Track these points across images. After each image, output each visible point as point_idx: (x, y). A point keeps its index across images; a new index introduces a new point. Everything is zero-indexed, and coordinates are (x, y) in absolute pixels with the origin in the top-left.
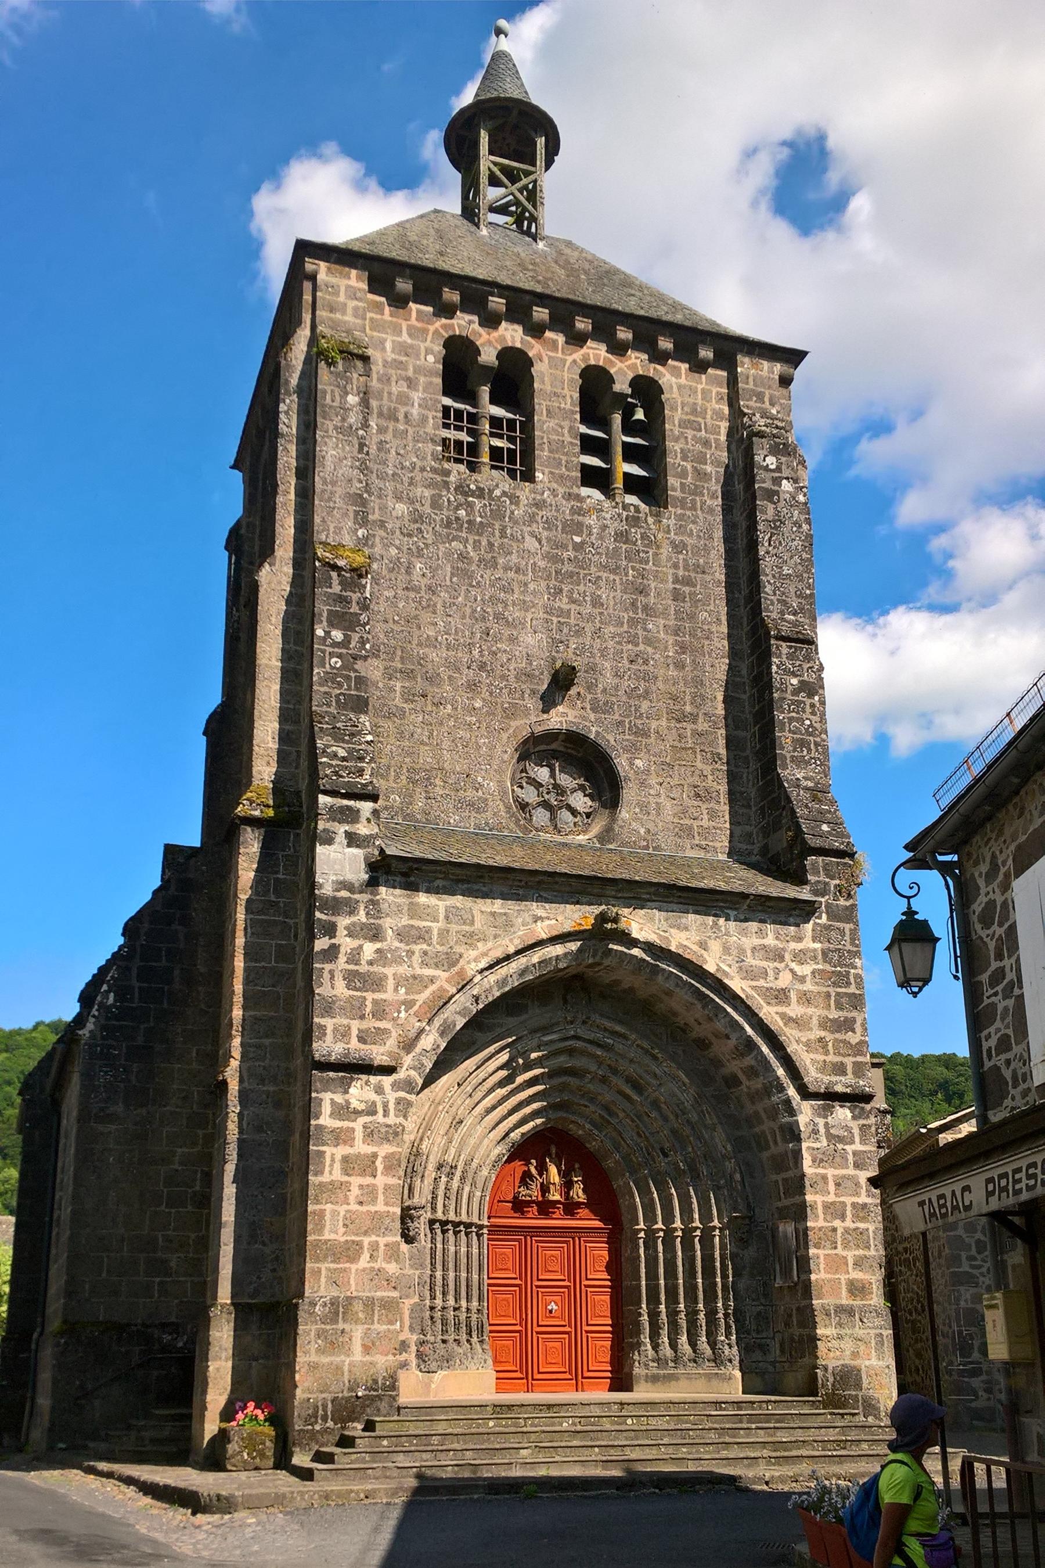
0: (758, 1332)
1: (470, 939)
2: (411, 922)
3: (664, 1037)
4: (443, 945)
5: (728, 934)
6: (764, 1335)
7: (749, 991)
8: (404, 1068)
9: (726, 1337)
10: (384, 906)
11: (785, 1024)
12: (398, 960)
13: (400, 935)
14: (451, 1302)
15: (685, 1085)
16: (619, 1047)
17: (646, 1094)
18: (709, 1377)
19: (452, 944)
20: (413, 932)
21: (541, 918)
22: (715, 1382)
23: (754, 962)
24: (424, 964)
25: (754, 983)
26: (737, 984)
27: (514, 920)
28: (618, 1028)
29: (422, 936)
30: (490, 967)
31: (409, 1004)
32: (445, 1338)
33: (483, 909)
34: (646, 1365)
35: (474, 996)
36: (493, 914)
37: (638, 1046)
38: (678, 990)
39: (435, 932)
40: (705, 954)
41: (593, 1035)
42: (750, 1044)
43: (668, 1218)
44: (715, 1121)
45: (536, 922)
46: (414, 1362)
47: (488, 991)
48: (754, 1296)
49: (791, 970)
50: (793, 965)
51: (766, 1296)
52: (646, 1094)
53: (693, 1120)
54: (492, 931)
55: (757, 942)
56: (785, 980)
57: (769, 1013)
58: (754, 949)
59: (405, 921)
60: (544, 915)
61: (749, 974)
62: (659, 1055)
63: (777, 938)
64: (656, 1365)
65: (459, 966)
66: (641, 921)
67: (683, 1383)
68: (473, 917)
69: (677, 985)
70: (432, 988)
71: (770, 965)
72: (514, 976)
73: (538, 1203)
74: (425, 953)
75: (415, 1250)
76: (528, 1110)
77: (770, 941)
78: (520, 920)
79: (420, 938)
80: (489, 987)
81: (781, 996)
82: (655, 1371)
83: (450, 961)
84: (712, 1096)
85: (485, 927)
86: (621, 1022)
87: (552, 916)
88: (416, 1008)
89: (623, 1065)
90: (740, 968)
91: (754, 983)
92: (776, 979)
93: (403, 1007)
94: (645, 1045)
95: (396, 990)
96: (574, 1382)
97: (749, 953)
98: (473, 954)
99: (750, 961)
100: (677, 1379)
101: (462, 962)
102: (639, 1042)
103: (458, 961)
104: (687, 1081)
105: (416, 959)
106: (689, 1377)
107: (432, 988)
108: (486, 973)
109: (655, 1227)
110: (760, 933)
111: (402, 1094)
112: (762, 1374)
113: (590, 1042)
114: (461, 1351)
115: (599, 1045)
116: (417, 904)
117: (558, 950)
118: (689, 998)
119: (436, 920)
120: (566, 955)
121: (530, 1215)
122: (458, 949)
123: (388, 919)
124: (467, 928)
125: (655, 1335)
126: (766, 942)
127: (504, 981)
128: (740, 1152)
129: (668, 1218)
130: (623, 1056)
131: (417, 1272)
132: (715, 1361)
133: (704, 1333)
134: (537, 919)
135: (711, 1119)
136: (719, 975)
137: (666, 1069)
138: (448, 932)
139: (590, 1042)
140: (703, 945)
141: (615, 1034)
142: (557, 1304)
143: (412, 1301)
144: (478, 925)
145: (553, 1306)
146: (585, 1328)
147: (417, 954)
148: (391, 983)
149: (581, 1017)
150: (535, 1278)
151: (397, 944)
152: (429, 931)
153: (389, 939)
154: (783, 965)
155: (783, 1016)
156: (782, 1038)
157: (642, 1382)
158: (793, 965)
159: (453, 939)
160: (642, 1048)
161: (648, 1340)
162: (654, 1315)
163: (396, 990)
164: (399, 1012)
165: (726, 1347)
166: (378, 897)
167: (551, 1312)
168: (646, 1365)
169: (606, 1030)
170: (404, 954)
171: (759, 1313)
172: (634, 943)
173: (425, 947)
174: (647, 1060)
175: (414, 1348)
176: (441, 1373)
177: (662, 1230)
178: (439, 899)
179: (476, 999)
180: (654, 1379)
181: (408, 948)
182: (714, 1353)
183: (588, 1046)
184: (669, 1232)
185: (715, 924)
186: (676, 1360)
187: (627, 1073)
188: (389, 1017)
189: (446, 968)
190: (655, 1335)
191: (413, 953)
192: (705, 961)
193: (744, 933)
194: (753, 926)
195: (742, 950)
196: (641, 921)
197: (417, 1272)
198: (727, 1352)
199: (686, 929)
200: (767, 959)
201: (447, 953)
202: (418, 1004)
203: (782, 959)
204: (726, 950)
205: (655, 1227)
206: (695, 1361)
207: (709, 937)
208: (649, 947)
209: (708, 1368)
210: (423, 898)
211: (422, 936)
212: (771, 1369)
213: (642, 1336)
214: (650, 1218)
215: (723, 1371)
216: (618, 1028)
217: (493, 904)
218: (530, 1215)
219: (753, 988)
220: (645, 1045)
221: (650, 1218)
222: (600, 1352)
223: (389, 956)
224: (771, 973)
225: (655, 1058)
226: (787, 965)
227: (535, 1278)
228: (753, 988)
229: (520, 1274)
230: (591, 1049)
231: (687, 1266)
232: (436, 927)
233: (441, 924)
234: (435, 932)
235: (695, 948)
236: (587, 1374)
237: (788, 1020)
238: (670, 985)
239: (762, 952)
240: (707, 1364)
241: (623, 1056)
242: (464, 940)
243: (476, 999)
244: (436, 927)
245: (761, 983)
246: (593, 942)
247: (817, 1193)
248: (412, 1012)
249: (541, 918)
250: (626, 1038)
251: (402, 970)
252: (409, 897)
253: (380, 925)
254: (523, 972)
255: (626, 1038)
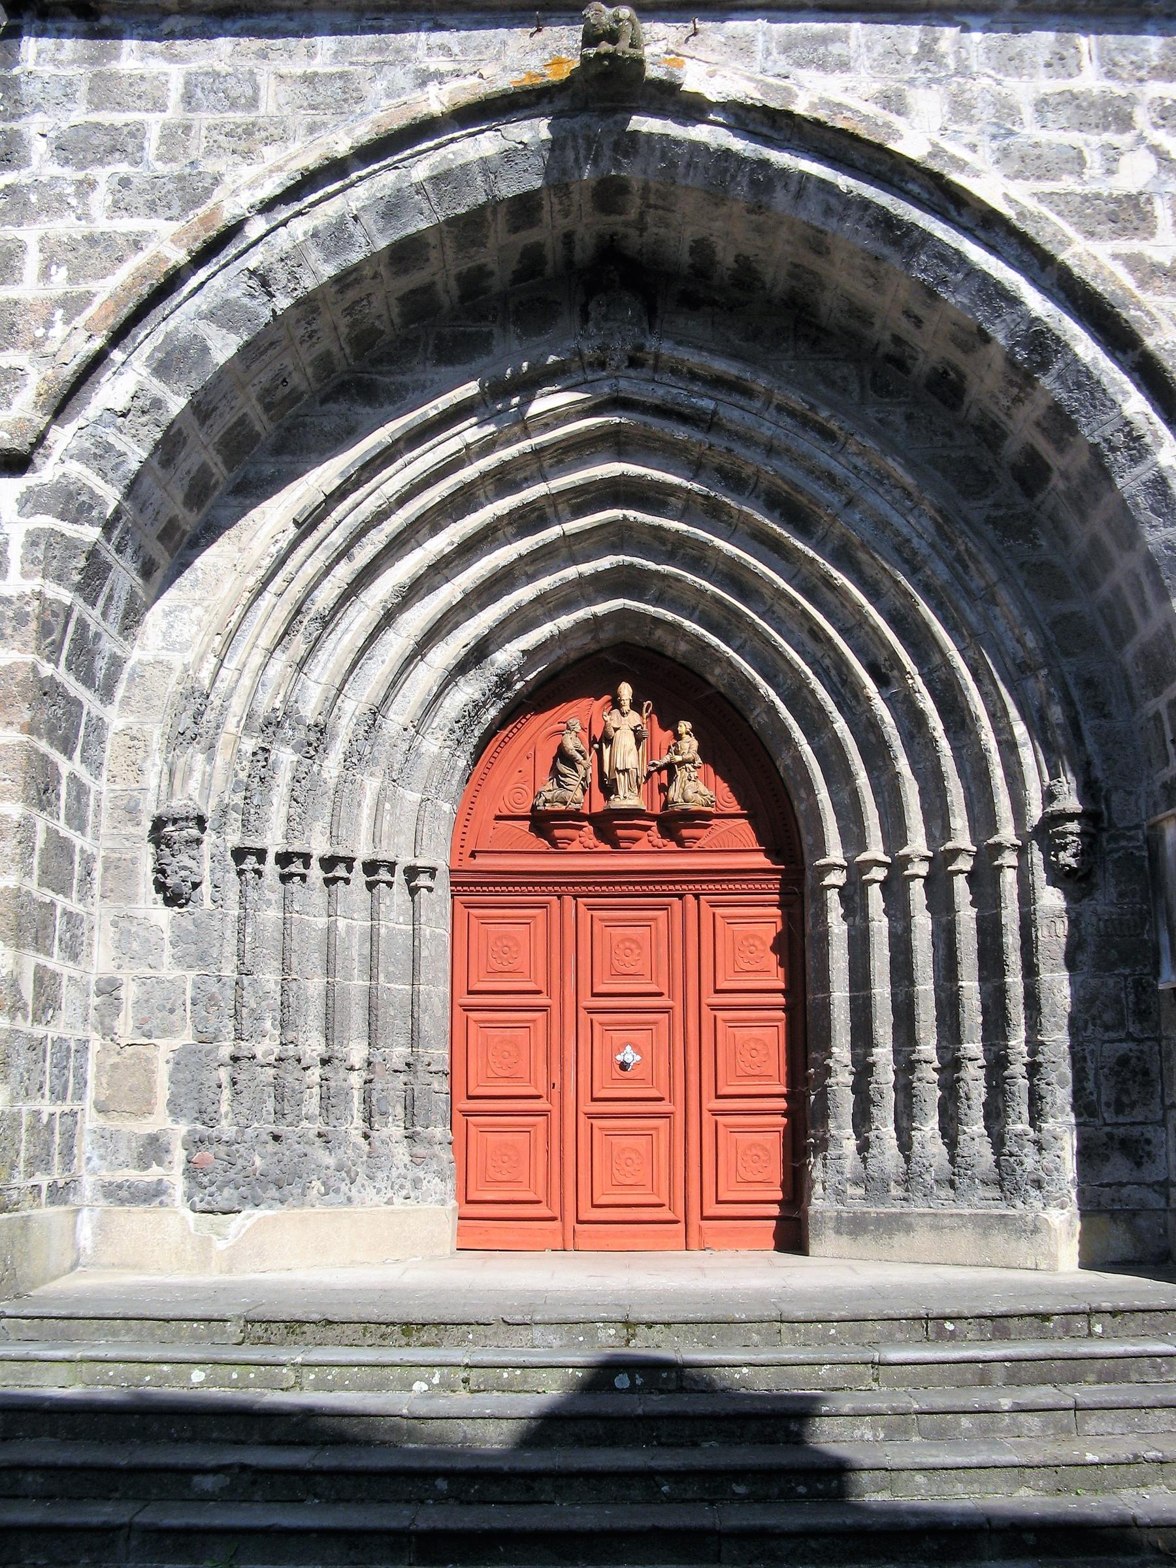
0: (1119, 1107)
1: (246, 140)
2: (95, 117)
3: (854, 386)
4: (173, 159)
5: (963, 70)
6: (1138, 1115)
7: (1032, 205)
8: (55, 458)
9: (1032, 1123)
10: (30, 90)
11: (1142, 284)
12: (55, 205)
13: (64, 149)
14: (313, 1046)
15: (909, 495)
16: (732, 414)
17: (820, 532)
18: (986, 1225)
19: (194, 155)
20: (98, 139)
21: (439, 76)
22: (998, 1239)
23: (1042, 136)
24: (118, 207)
25: (1047, 186)
26: (990, 187)
27: (365, 87)
28: (722, 366)
29: (119, 143)
30: (291, 194)
31: (73, 305)
32: (281, 1129)
33: (284, 71)
34: (840, 1194)
35: (253, 273)
36: (309, 79)
37: (780, 408)
38: (832, 224)
39: (153, 136)
40: (898, 122)
41: (661, 391)
42: (1042, 344)
43: (895, 833)
44: (992, 574)
45: (423, 84)
46: (178, 1183)
47: (293, 259)
48: (1108, 1017)
49: (1155, 150)
50: (1160, 137)
51: (1142, 1014)
52: (820, 532)
53: (937, 583)
54: (305, 117)
55: (1050, 85)
56: (1135, 173)
57: (1092, 257)
58: (1042, 105)
59: (79, 114)
60: (445, 65)
61: (1030, 164)
62: (833, 425)
63: (1110, 75)
64: (861, 1191)
65: (210, 203)
66: (713, 58)
67: (922, 1239)
68: (256, 89)
69: (828, 211)
70: (136, 261)
71: (1091, 142)
72: (365, 218)
73: (592, 818)
74: (125, 182)
75: (187, 923)
76: (525, 594)
77: (1090, 80)
78: (380, 85)
79: (113, 150)
80: (303, 251)
81: (1128, 214)
82: (859, 1207)
83: (192, 192)
84: (988, 520)
85: (287, 110)
86: (735, 356)
87: (466, 68)
88: (89, 312)
89: (751, 460)
90: (1005, 153)
91: (1047, 186)
92: (1110, 172)
93: (59, 313)
94: (796, 400)
95: (45, 274)
96: (681, 1226)
97: (1028, 113)
98: (247, 172)
99: (1030, 131)
100: (909, 1228)
101: (218, 194)
102: (778, 398)
103: (208, 192)
104: (908, 480)
105: (100, 199)
106: (936, 1224)
107: (136, 261)
108: (283, 212)
109: (864, 856)
110: (1059, 63)
111: (46, 521)
112: (1129, 1215)
113: (662, 411)
114: (330, 1160)
115: (683, 418)
116: (115, 77)
117: (481, 145)
118: (868, 242)
119: (159, 106)
120: (508, 156)
121: (575, 847)
122: (210, 166)
123: (39, 117)
124: (239, 117)
125: (862, 1118)
126: (1077, 84)
127: (335, 236)
128: (1067, 654)
129: (895, 833)
130: (747, 440)
131: (192, 975)
132: (1000, 1183)
133: (978, 1112)
134: (424, 78)
135: (982, 575)
136: (935, 166)
137: (859, 462)
138: (187, 129)
139: (662, 411)
140: (894, 102)
141: (718, 382)
142: (637, 1049)
143: (177, 1043)
144: (268, 105)
145: (629, 1055)
146: (712, 1104)
147: (102, 188)
148: (32, 262)
149: (620, 347)
150: (585, 990)
151: (55, 170)
152: (137, 132)
153: (35, 160)
154: (1128, 138)
155: (1133, 263)
156: (1130, 314)
157: (830, 1233)
158: (1160, 137)
159: (197, 146)
160: (792, 413)
161: (850, 1131)
162: (863, 1070)
163: (45, 274)
164: (48, 324)
165: (1030, 1149)
166: (16, 71)
167: (624, 1066)
168: (840, 1194)
169: (693, 376)
170: (70, 190)
171: (1123, 1061)
172: (693, 109)
173: (124, 168)
174: (807, 443)
175: (179, 1155)
176: (250, 1217)
177: (878, 863)
178: (174, 58)
179: (263, 279)
180: (855, 1226)
181: (80, 175)
182: (998, 1164)
183: (649, 419)
184: (897, 866)
185: (927, 51)
186: (907, 1180)
187: (764, 484)
188: (26, 338)
189: (175, 211)
190: (862, 1118)
191: (93, 185)
192: (897, 135)
193: (1013, 64)
194: (1043, 41)
195: (1006, 110)
196: (713, 58)
197: (192, 975)
198: (1029, 1163)
199: (844, 65)
200: (1081, 127)
201: (181, 178)
202: (97, 301)
203: (1124, 122)
204: (961, 109)
205: (864, 856)
206: (952, 1184)
207: (911, 82)
208: (745, 117)
209: (981, 1201)
210: (132, 57)
211: (119, 143)
212: (1154, 1200)
213: (831, 1124)
214: (854, 838)
215: (1019, 1209)
216: (722, 366)
217: (311, 55)
218: (575, 847)
219: (1041, 197)
220: (796, 400)
221: (854, 838)
222: (753, 1159)
223: (33, 198)
224: (1094, 159)
225: (827, 435)
226: (1141, 139)
227: (585, 990)
228: (1041, 197)
229: (548, 983)
230: (657, 425)
231: (941, 946)
232: (154, 123)
233: (174, 112)
234: (153, 136)
235: (871, 109)
236: (712, 1209)
237: (1149, 272)
238: (811, 212)
239: (1069, 111)
240: (982, 1191)
241: (747, 440)
242: (232, 143)
243: (263, 279)
244: (154, 123)
245: (1067, 183)
246: (583, 119)
247: (67, 161)
248: (79, 321)
249: (439, 76)
250: (747, 392)
251: (65, 226)
252: (93, 61)
253: (17, 134)
254: (392, 209)
255: (747, 392)
